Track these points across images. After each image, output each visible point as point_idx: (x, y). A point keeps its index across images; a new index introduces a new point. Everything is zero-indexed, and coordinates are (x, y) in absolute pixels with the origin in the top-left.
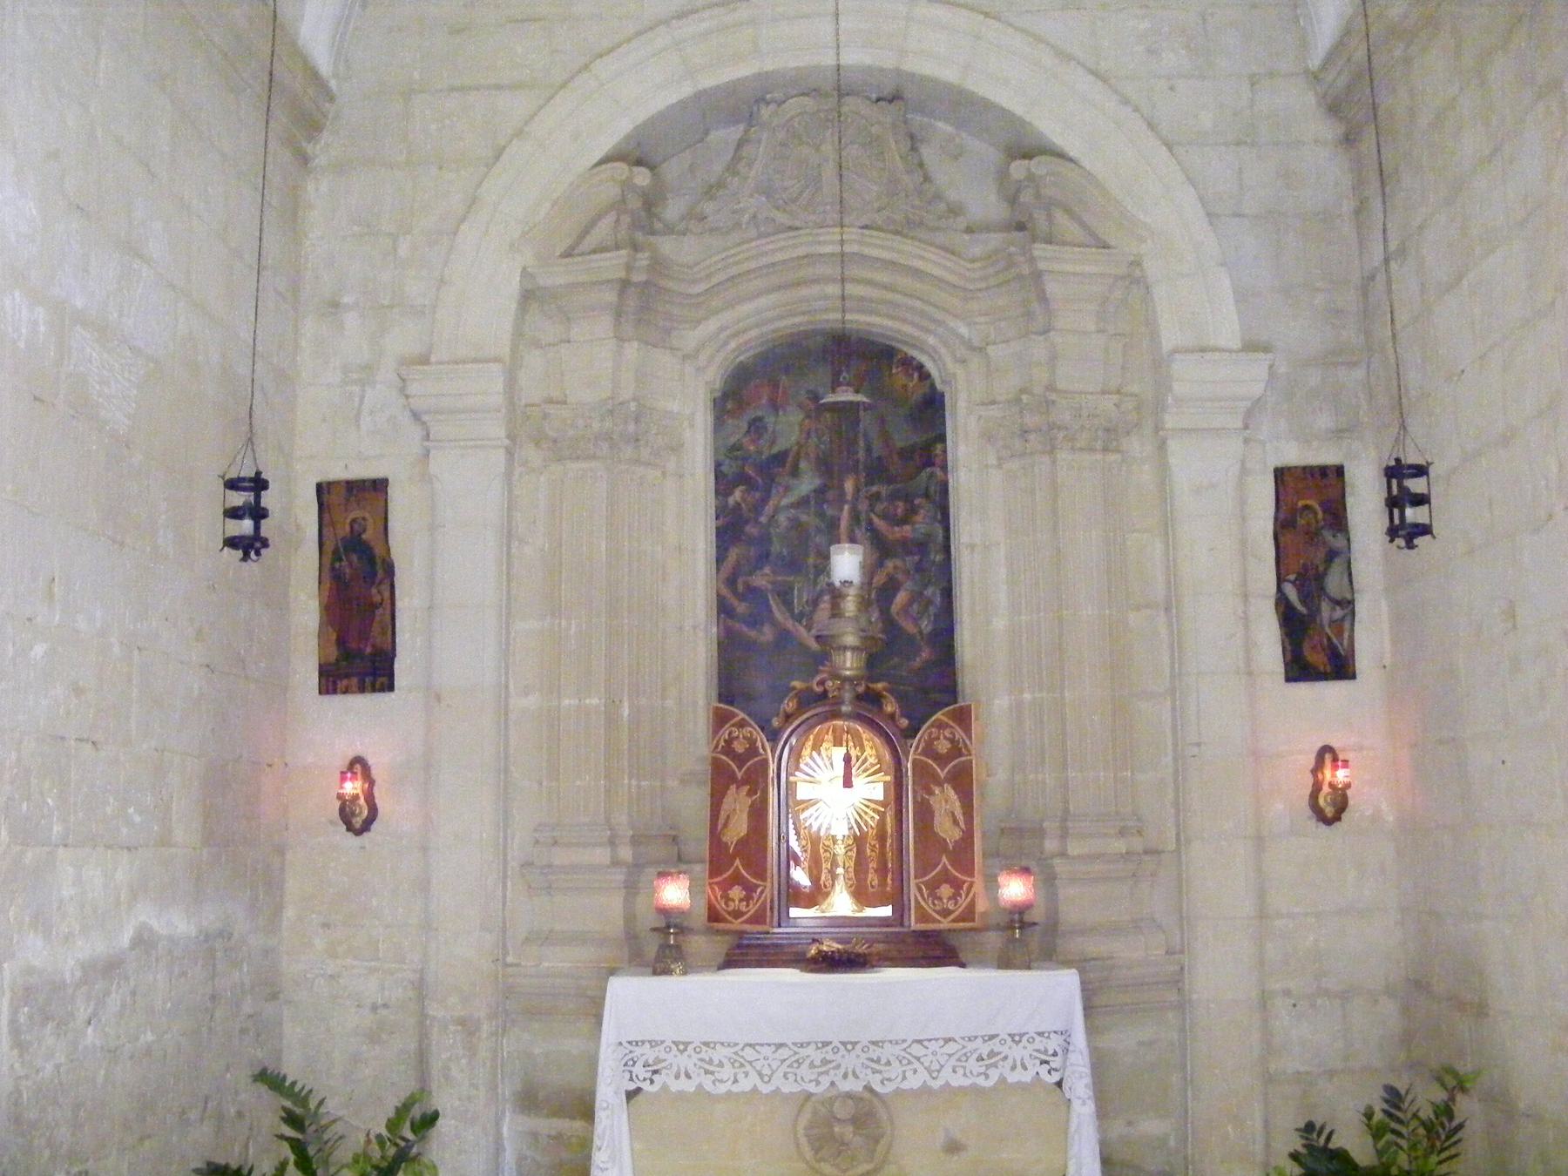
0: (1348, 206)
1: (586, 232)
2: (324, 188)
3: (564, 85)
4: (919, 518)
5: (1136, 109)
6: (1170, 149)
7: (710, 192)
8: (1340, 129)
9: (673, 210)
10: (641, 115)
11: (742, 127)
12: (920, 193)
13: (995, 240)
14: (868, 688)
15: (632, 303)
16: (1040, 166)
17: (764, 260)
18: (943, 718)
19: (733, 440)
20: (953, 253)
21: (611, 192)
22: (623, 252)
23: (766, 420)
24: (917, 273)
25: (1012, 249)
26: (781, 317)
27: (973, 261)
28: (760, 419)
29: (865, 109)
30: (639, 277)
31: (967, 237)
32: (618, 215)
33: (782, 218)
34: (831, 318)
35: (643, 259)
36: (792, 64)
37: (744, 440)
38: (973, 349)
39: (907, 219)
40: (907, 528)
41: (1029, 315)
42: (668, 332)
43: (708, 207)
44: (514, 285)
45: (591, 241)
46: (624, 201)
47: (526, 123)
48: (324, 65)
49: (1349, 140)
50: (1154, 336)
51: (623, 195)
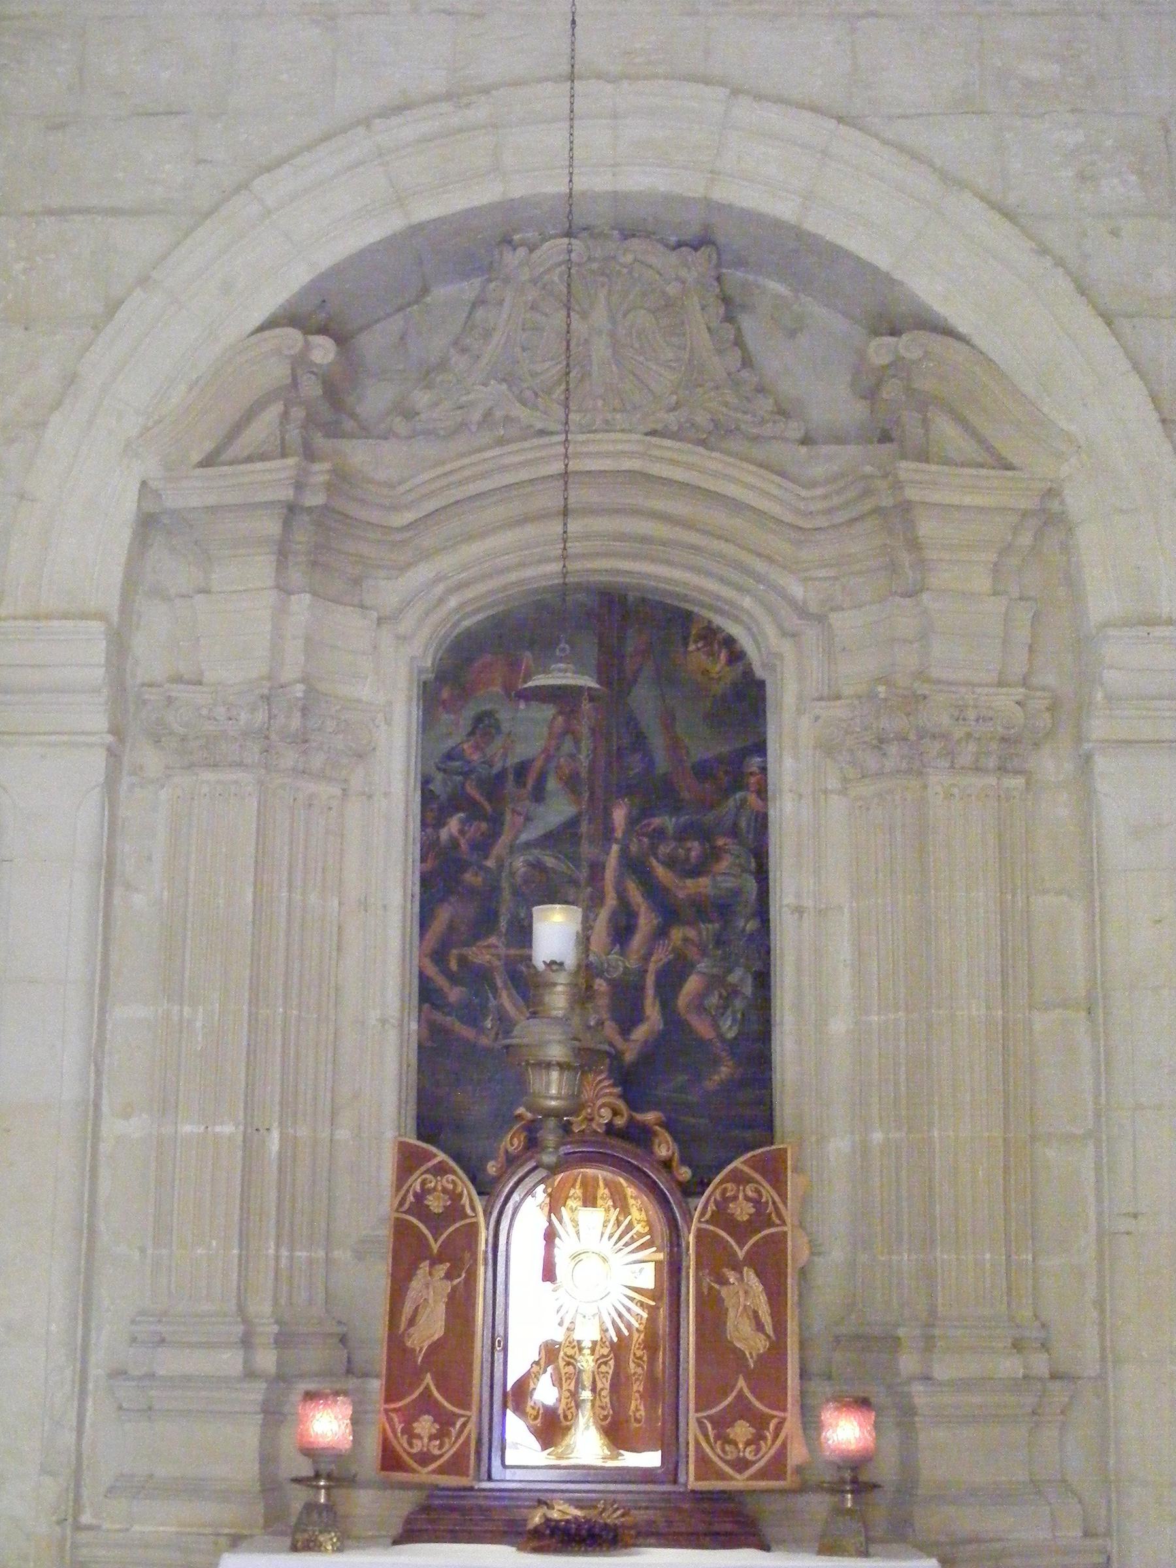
4: (724, 865)
5: (1060, 262)
6: (1109, 324)
10: (327, 256)
12: (736, 384)
15: (302, 537)
16: (908, 346)
18: (746, 1169)
19: (450, 743)
21: (279, 372)
27: (813, 484)
28: (489, 714)
30: (315, 499)
31: (803, 450)
33: (521, 412)
35: (320, 472)
37: (465, 746)
40: (704, 881)
41: (893, 568)
42: (357, 581)
43: (422, 399)
44: (129, 506)
46: (295, 384)
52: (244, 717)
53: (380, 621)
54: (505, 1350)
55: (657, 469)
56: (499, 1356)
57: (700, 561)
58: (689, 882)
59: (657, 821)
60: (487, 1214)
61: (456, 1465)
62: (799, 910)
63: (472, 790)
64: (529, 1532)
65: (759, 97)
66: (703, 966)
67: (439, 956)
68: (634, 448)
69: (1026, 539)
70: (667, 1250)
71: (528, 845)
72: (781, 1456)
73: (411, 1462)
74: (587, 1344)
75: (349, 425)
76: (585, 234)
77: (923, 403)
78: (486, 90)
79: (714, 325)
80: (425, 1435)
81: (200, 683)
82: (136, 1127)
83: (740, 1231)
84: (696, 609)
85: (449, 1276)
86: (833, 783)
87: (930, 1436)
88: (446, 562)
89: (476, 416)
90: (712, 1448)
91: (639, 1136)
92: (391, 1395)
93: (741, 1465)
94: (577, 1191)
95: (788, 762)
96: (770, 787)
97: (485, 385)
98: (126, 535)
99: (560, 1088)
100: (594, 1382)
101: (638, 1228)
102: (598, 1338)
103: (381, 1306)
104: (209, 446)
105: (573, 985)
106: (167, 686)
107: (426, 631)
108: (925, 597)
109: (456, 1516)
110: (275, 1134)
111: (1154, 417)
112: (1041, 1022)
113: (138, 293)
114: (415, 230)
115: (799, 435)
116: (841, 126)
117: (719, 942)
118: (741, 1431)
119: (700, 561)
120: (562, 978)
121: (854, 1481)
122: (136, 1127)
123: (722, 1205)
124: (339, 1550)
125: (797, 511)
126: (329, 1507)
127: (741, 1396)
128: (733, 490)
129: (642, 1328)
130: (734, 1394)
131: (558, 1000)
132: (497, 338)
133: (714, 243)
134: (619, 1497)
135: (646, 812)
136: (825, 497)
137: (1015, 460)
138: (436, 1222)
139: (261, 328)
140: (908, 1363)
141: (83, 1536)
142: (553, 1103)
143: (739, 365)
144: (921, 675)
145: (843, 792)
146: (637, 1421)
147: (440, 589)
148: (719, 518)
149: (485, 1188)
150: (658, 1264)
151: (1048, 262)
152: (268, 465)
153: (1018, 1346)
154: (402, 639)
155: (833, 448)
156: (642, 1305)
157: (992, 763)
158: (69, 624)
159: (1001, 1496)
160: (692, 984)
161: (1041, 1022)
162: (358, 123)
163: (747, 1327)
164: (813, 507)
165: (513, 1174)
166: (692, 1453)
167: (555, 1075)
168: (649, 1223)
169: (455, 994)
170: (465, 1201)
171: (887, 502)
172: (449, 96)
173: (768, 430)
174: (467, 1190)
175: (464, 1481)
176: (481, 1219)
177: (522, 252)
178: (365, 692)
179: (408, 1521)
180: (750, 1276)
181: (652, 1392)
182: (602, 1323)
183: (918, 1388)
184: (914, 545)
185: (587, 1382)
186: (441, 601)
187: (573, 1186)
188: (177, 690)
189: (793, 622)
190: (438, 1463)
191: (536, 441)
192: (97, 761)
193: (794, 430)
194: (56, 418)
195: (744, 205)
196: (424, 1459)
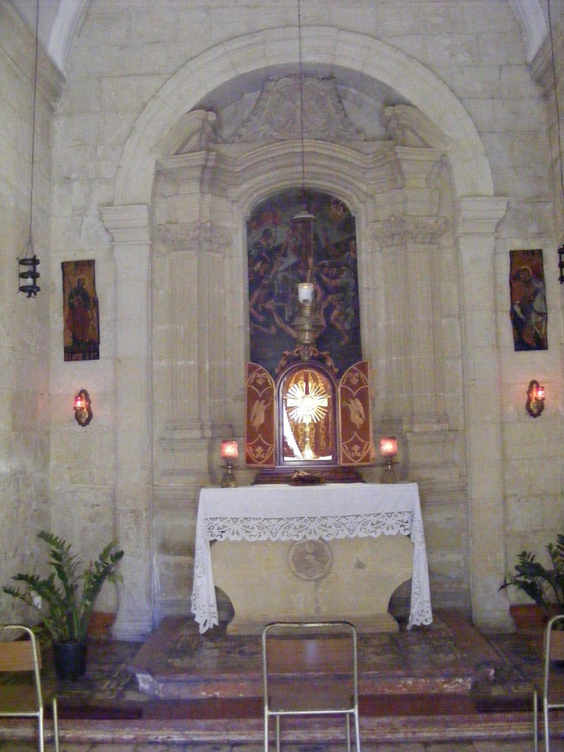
0: (544, 128)
2: (62, 123)
3: (174, 74)
5: (445, 82)
6: (461, 101)
9: (227, 132)
10: (211, 86)
14: (319, 354)
15: (207, 176)
16: (398, 110)
17: (269, 156)
19: (256, 240)
21: (197, 124)
22: (204, 152)
23: (271, 230)
24: (340, 160)
30: (211, 164)
31: (365, 143)
32: (201, 135)
34: (299, 183)
35: (212, 155)
41: (394, 180)
43: (243, 130)
44: (152, 170)
48: (60, 65)
51: (203, 125)
52: (192, 234)
53: (233, 202)
54: (283, 426)
55: (318, 150)
56: (281, 428)
58: (333, 281)
59: (323, 262)
60: (276, 383)
61: (269, 461)
62: (368, 289)
63: (264, 255)
64: (293, 480)
66: (338, 307)
67: (255, 307)
70: (331, 394)
71: (281, 271)
72: (368, 455)
73: (255, 461)
74: (307, 424)
75: (220, 140)
78: (261, 31)
79: (335, 104)
80: (260, 453)
81: (177, 223)
82: (163, 364)
83: (354, 387)
84: (331, 194)
85: (265, 404)
86: (378, 249)
87: (413, 449)
90: (347, 453)
91: (322, 359)
92: (249, 441)
93: (356, 458)
94: (302, 378)
95: (364, 243)
96: (358, 251)
98: (152, 177)
99: (309, 338)
100: (310, 436)
101: (322, 388)
102: (311, 422)
103: (243, 414)
104: (176, 148)
105: (311, 307)
106: (167, 225)
107: (247, 205)
108: (405, 189)
109: (270, 476)
110: (207, 363)
112: (444, 321)
115: (363, 138)
117: (343, 299)
118: (356, 448)
120: (308, 305)
121: (391, 461)
122: (163, 364)
123: (348, 379)
124: (236, 487)
126: (232, 474)
127: (356, 438)
128: (343, 157)
129: (324, 419)
130: (353, 437)
131: (307, 311)
133: (334, 78)
134: (319, 469)
135: (318, 260)
136: (373, 158)
138: (260, 388)
140: (405, 427)
141: (156, 488)
142: (307, 342)
144: (404, 214)
145: (381, 251)
146: (323, 447)
147: (250, 191)
149: (276, 377)
150: (328, 399)
152: (195, 154)
153: (438, 422)
154: (240, 207)
156: (324, 412)
157: (427, 241)
158: (136, 206)
159: (434, 467)
160: (335, 312)
161: (444, 321)
163: (357, 417)
165: (283, 372)
166: (341, 454)
167: (307, 333)
168: (325, 386)
169: (261, 318)
170: (269, 381)
174: (270, 379)
175: (273, 466)
176: (275, 388)
177: (273, 83)
178: (228, 224)
179: (256, 478)
180: (357, 401)
181: (327, 439)
182: (312, 418)
183: (409, 434)
184: (401, 173)
185: (308, 436)
186: (252, 195)
187: (301, 376)
188: (169, 226)
190: (264, 461)
191: (281, 143)
192: (146, 250)
193: (362, 137)
196: (259, 460)
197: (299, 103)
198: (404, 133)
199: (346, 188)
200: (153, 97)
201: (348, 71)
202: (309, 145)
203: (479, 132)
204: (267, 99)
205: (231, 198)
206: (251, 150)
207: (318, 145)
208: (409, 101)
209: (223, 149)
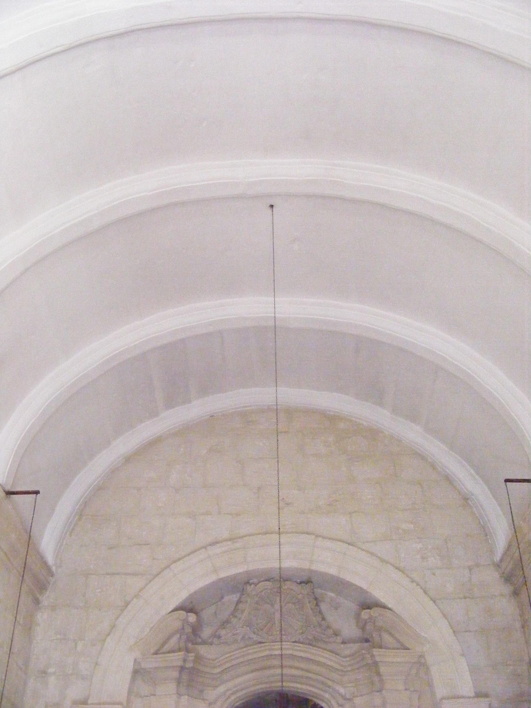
0: (518, 625)
1: (163, 645)
2: (45, 616)
3: (158, 575)
5: (418, 584)
6: (434, 602)
7: (225, 624)
8: (512, 588)
9: (206, 632)
10: (193, 589)
11: (238, 595)
12: (320, 625)
13: (355, 647)
15: (185, 677)
16: (375, 612)
17: (246, 658)
20: (336, 654)
21: (178, 624)
22: (182, 653)
24: (318, 663)
25: (364, 652)
26: (254, 685)
27: (345, 657)
29: (295, 587)
30: (189, 665)
31: (342, 646)
32: (180, 636)
33: (255, 637)
34: (276, 686)
35: (191, 656)
36: (262, 567)
38: (346, 699)
39: (314, 638)
41: (372, 683)
42: (201, 691)
43: (223, 632)
44: (130, 666)
45: (167, 648)
46: (183, 628)
47: (140, 591)
48: (50, 559)
49: (516, 593)
50: (433, 694)
51: (183, 626)
57: (312, 683)
65: (324, 538)
68: (289, 647)
69: (414, 671)
76: (272, 580)
77: (380, 629)
88: (230, 684)
89: (240, 638)
97: (243, 627)
98: (129, 677)
104: (155, 648)
111: (451, 631)
113: (135, 600)
114: (222, 580)
116: (349, 546)
119: (312, 683)
125: (342, 666)
128: (321, 659)
132: (246, 613)
133: (312, 582)
137: (410, 647)
139: (172, 611)
143: (321, 619)
148: (314, 667)
151: (415, 584)
155: (351, 645)
162: (202, 548)
164: (346, 664)
171: (370, 661)
172: (230, 539)
173: (331, 640)
184: (378, 674)
189: (341, 701)
191: (260, 645)
193: (339, 639)
194: (108, 640)
195: (321, 570)
197: (277, 606)
198: (380, 635)
199: (325, 691)
200: (137, 596)
201: (324, 575)
202: (289, 649)
203: (454, 632)
204: (246, 602)
205: (207, 700)
206: (230, 652)
207: (296, 648)
208: (384, 603)
209: (203, 650)
